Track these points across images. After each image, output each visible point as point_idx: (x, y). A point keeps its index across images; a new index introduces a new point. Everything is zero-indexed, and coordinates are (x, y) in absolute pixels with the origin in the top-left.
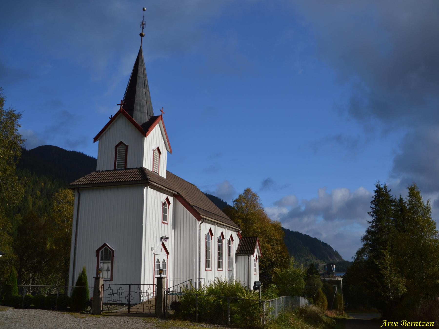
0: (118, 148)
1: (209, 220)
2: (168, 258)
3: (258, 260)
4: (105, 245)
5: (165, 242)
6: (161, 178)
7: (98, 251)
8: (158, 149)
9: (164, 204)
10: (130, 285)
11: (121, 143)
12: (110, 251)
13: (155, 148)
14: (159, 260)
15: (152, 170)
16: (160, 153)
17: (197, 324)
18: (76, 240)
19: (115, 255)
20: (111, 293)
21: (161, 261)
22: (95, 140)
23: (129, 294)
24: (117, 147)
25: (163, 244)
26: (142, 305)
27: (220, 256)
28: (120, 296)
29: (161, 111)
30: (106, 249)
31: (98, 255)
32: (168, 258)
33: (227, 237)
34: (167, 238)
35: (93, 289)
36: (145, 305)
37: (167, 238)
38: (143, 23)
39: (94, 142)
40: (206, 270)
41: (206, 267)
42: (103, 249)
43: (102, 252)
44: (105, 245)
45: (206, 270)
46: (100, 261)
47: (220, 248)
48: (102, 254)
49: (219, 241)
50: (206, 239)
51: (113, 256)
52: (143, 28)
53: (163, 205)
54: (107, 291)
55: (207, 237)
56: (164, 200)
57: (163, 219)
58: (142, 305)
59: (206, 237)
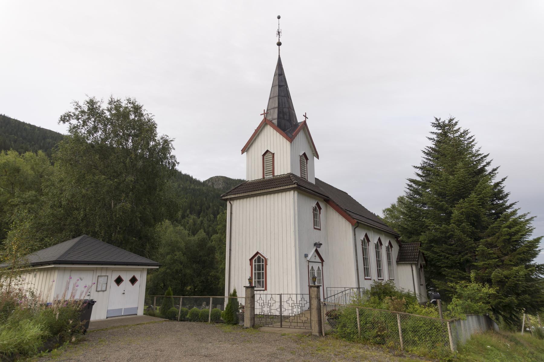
0: (265, 157)
1: (365, 260)
2: (322, 265)
3: (423, 269)
4: (258, 253)
5: (318, 249)
6: (310, 184)
7: (251, 260)
8: (304, 154)
9: (315, 210)
10: (281, 295)
11: (267, 151)
12: (263, 260)
13: (301, 154)
14: (314, 268)
15: (299, 175)
16: (307, 159)
17: (360, 345)
18: (230, 250)
19: (268, 263)
21: (316, 269)
22: (243, 151)
23: (281, 305)
24: (264, 155)
26: (296, 318)
28: (272, 308)
29: (305, 116)
30: (259, 258)
31: (251, 264)
32: (322, 265)
33: (385, 243)
34: (321, 244)
35: (244, 299)
36: (298, 318)
37: (321, 244)
38: (279, 33)
40: (366, 279)
41: (365, 276)
43: (255, 260)
45: (366, 279)
47: (378, 254)
48: (255, 262)
50: (362, 245)
51: (266, 264)
52: (279, 37)
53: (314, 210)
54: (258, 301)
56: (314, 204)
57: (314, 225)
58: (296, 318)
59: (362, 242)
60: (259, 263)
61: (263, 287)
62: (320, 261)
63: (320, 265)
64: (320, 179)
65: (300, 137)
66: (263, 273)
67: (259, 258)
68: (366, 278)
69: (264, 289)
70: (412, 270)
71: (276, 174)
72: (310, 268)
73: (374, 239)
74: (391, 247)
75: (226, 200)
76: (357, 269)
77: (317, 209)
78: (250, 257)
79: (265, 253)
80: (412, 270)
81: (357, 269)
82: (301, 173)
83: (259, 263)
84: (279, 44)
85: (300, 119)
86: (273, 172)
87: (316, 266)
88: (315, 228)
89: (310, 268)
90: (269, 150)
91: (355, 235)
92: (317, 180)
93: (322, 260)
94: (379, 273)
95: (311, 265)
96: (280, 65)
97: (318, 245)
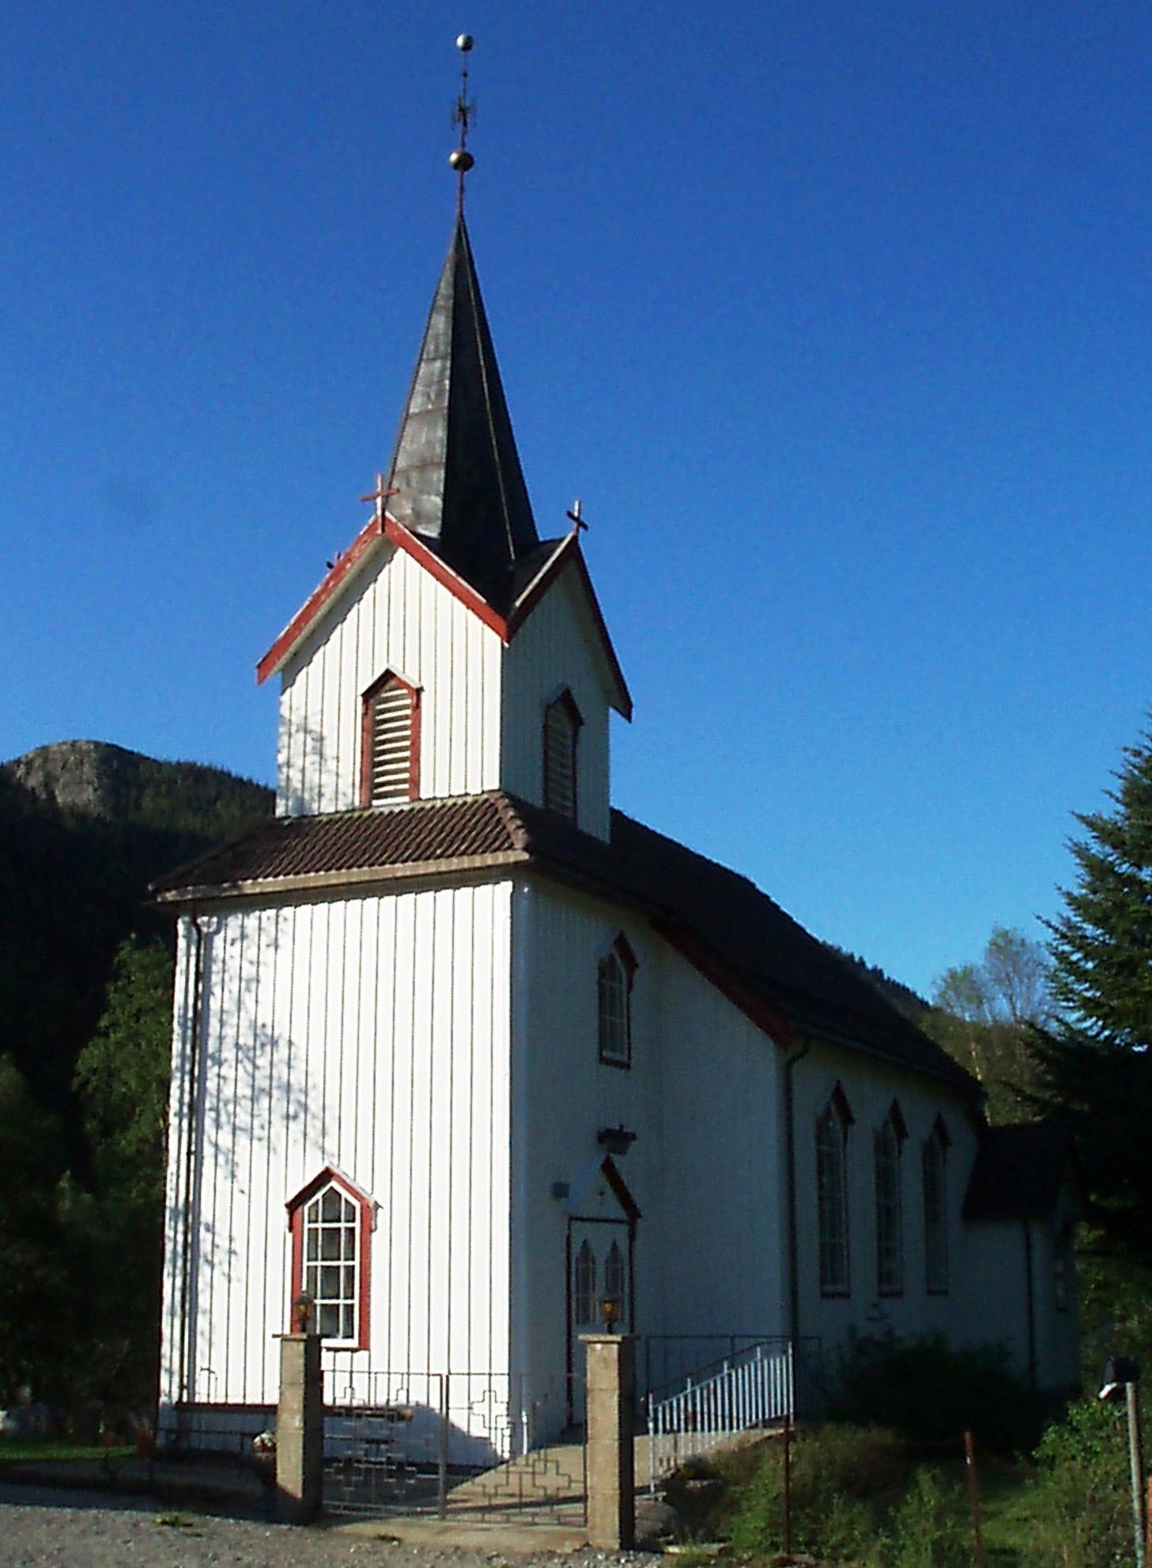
2: (632, 1237)
4: (326, 1175)
5: (616, 1159)
7: (293, 1206)
9: (606, 970)
11: (388, 675)
14: (593, 1245)
16: (577, 721)
20: (540, 1466)
24: (370, 695)
25: (608, 1168)
27: (887, 1215)
32: (632, 1237)
33: (919, 1128)
38: (463, 111)
39: (261, 679)
41: (823, 1282)
42: (319, 1196)
44: (824, 1295)
46: (574, 1326)
47: (886, 1180)
49: (883, 1148)
51: (368, 1229)
52: (464, 133)
55: (822, 1127)
60: (331, 1225)
61: (349, 1335)
62: (622, 1214)
63: (623, 1230)
64: (629, 813)
65: (555, 614)
66: (350, 1270)
67: (333, 1197)
68: (829, 1288)
69: (353, 1343)
70: (1028, 1247)
71: (424, 794)
72: (576, 1248)
73: (871, 1101)
74: (945, 1141)
75: (177, 909)
76: (794, 1293)
77: (615, 973)
78: (291, 1196)
79: (358, 1173)
80: (1028, 1247)
81: (794, 1293)
82: (546, 790)
83: (331, 1225)
84: (465, 75)
85: (549, 524)
86: (415, 782)
87: (602, 1240)
88: (603, 1060)
89: (576, 1248)
90: (397, 670)
91: (787, 1091)
92: (616, 815)
93: (632, 1212)
94: (888, 1283)
95: (581, 1232)
96: (462, 232)
97: (615, 1139)
